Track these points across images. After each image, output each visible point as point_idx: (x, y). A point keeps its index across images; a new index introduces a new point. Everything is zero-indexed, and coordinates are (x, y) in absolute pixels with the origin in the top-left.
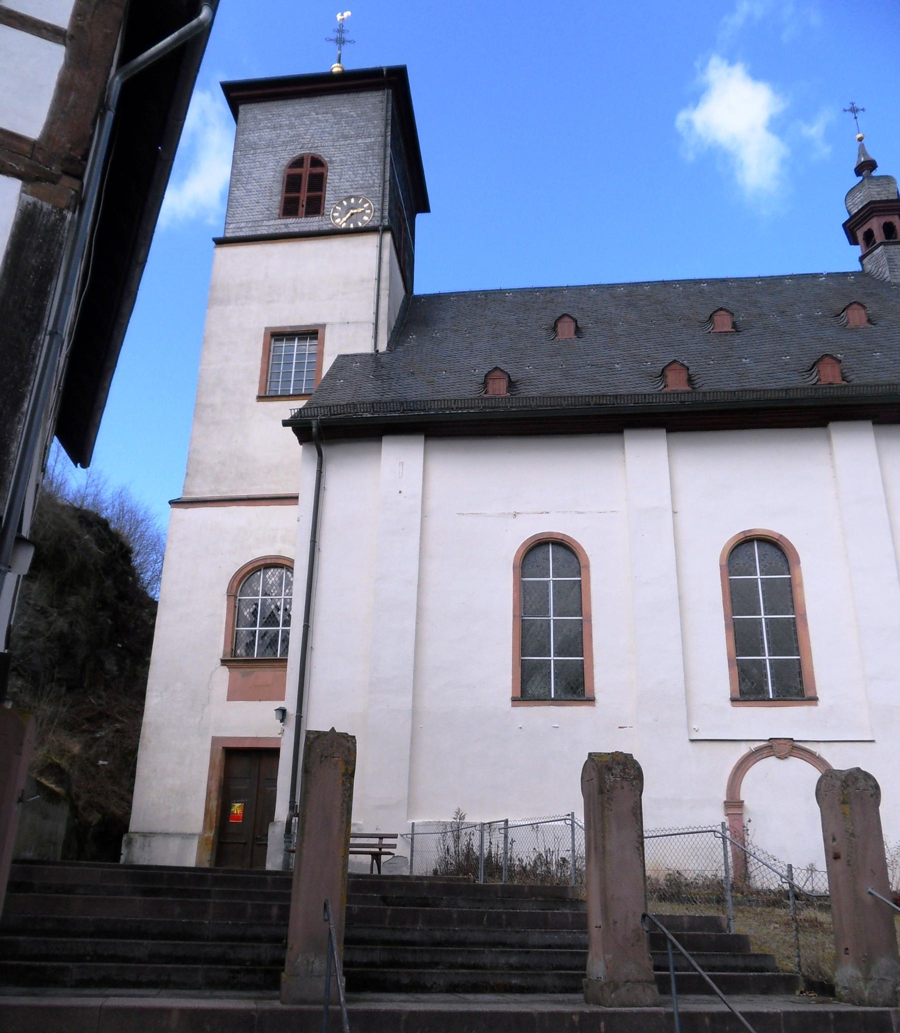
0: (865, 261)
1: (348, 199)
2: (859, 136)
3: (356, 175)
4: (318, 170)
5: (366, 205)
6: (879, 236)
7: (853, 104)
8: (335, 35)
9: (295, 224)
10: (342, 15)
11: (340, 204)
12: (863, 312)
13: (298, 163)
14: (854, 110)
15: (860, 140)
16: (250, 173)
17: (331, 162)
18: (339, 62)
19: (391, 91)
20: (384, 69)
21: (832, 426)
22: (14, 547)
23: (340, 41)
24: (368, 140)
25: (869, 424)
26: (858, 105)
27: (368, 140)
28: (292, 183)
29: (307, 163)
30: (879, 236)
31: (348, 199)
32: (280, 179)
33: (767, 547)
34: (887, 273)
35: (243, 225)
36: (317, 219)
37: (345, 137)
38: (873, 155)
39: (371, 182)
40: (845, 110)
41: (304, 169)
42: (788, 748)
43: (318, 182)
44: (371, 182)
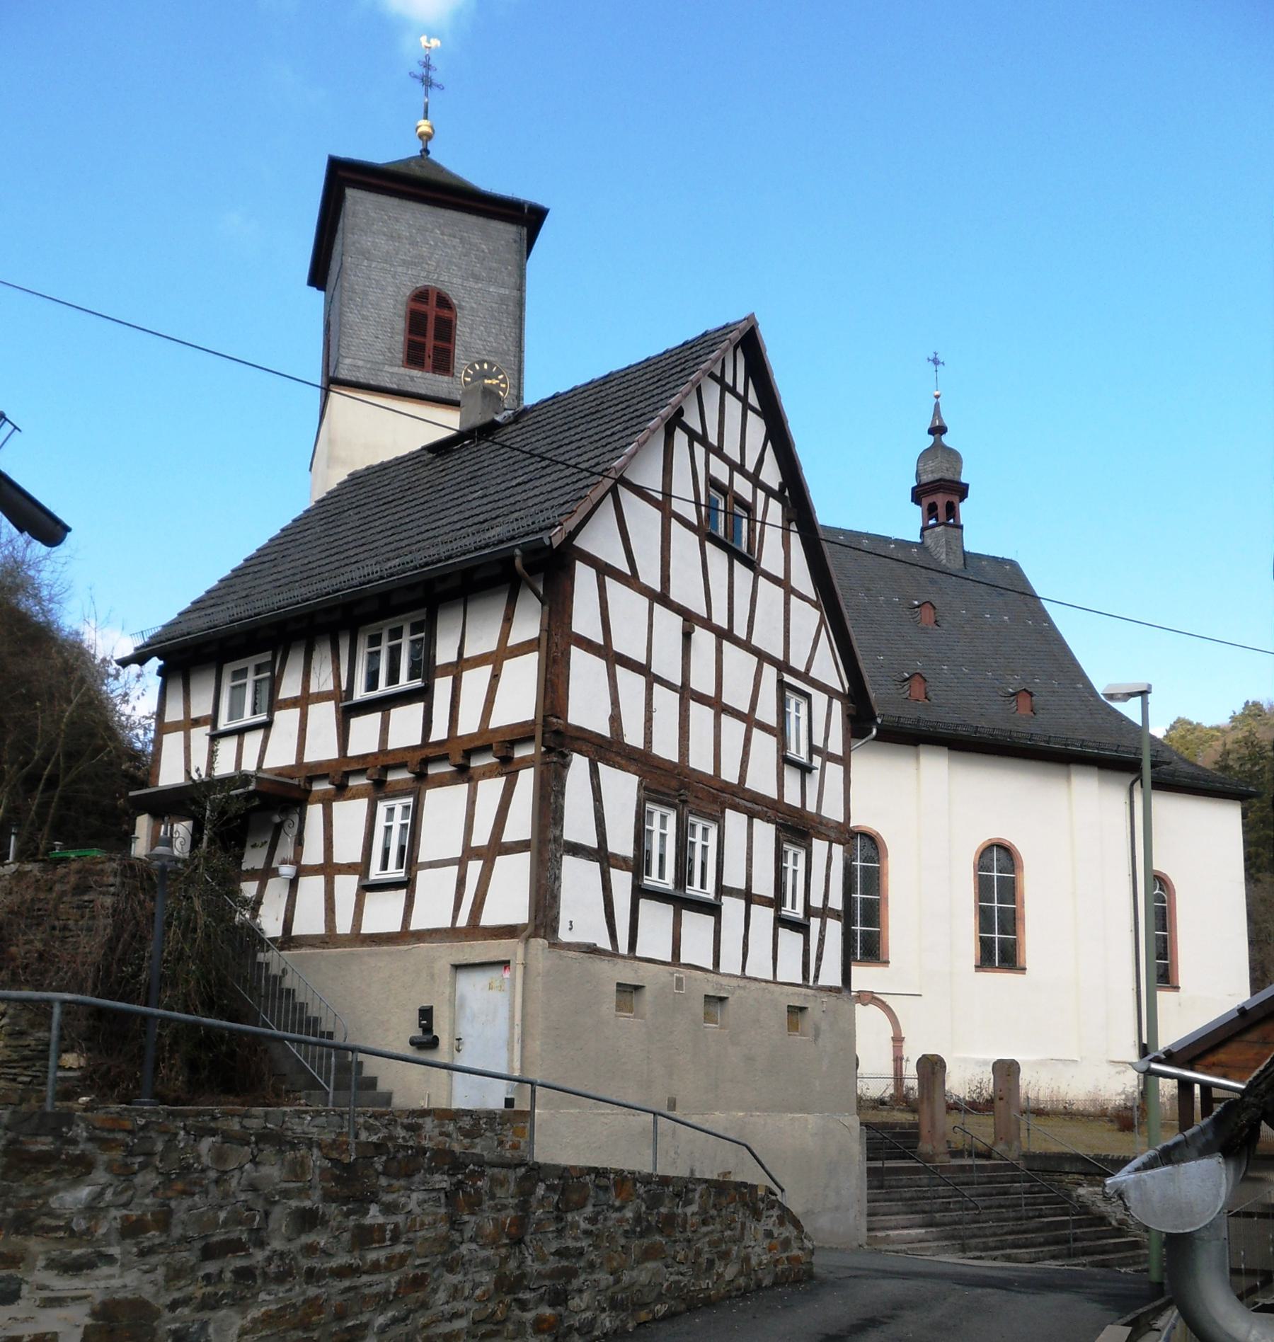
0: (926, 533)
1: (481, 363)
2: (937, 393)
3: (489, 334)
4: (445, 313)
5: (501, 377)
6: (941, 511)
7: (936, 354)
8: (420, 71)
9: (422, 380)
10: (429, 42)
11: (472, 367)
12: (932, 612)
13: (421, 296)
14: (936, 362)
15: (937, 397)
16: (365, 293)
17: (462, 308)
18: (426, 118)
19: (525, 229)
20: (526, 207)
21: (922, 747)
22: (1131, 1161)
23: (427, 82)
24: (502, 291)
25: (946, 749)
26: (941, 358)
27: (502, 291)
28: (416, 322)
29: (433, 300)
30: (941, 511)
31: (481, 363)
32: (403, 313)
33: (866, 840)
34: (943, 556)
35: (360, 363)
36: (446, 378)
37: (477, 278)
38: (947, 422)
39: (505, 347)
40: (929, 360)
41: (429, 307)
42: (870, 998)
43: (446, 330)
44: (505, 347)
